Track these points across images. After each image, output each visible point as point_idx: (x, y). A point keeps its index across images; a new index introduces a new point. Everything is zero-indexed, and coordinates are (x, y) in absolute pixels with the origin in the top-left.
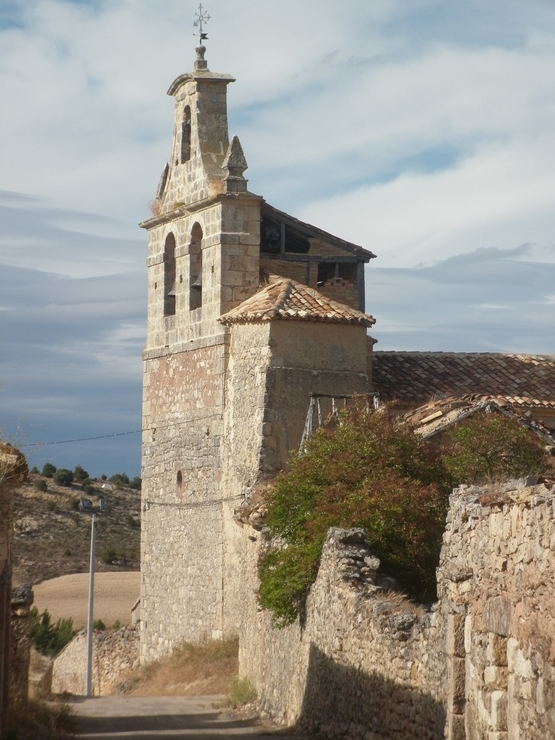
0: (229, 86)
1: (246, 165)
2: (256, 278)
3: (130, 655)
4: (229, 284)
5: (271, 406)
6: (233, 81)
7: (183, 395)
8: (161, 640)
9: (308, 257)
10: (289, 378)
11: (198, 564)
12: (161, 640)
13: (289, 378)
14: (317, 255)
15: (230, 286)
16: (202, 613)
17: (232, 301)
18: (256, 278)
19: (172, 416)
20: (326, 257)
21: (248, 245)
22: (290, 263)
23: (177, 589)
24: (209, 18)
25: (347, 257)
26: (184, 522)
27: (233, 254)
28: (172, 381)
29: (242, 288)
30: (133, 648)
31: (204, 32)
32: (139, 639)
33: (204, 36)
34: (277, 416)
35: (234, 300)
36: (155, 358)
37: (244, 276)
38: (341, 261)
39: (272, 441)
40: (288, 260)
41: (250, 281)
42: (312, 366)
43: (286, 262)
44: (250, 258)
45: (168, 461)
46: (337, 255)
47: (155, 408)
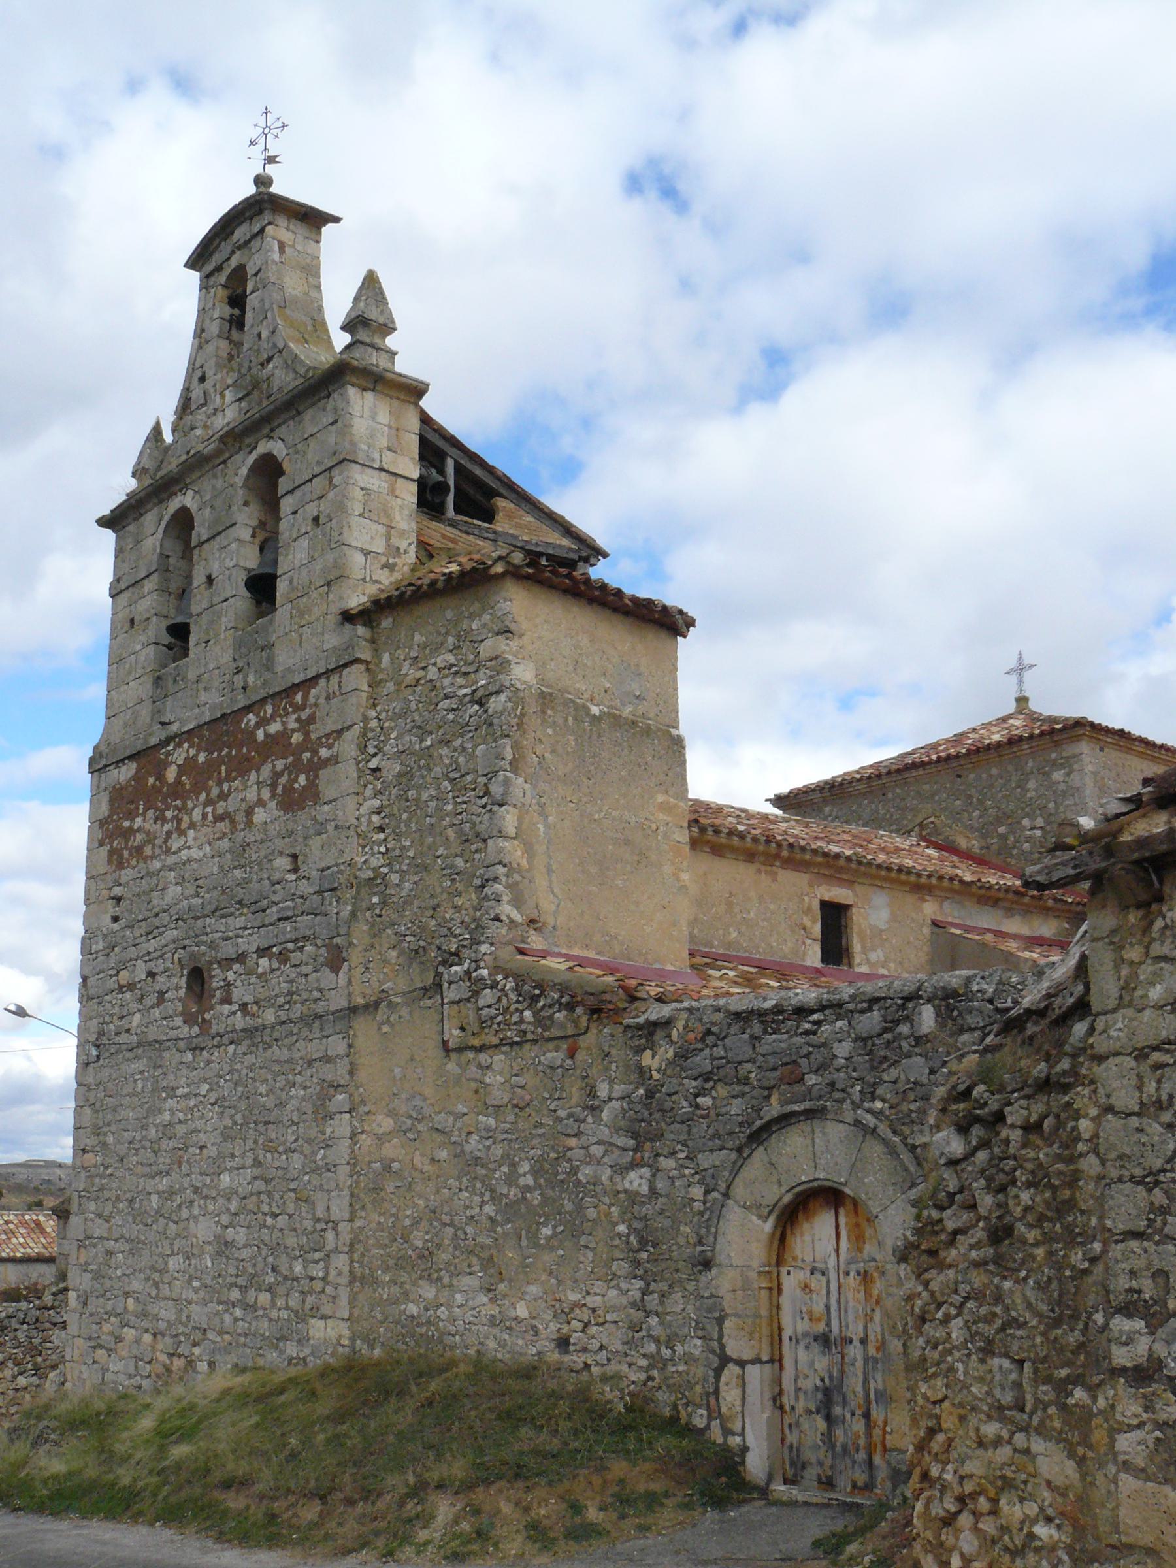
0: (328, 230)
1: (393, 322)
2: (410, 544)
3: (39, 1359)
4: (359, 545)
5: (517, 768)
6: (337, 220)
7: (209, 809)
8: (129, 1333)
9: (495, 532)
10: (549, 712)
11: (257, 1163)
12: (129, 1333)
13: (549, 712)
14: (511, 532)
15: (362, 550)
16: (270, 1278)
17: (364, 579)
18: (410, 544)
19: (171, 860)
20: (526, 538)
21: (395, 475)
22: (463, 535)
23: (182, 1225)
24: (284, 126)
25: (560, 546)
26: (209, 1074)
27: (368, 486)
28: (176, 791)
29: (384, 559)
30: (49, 1345)
31: (271, 153)
32: (64, 1328)
33: (271, 160)
34: (528, 793)
35: (368, 579)
36: (123, 760)
37: (388, 537)
38: (551, 552)
39: (519, 853)
40: (461, 531)
41: (398, 549)
42: (586, 696)
43: (458, 532)
44: (399, 501)
45: (159, 953)
46: (544, 540)
47: (121, 856)
